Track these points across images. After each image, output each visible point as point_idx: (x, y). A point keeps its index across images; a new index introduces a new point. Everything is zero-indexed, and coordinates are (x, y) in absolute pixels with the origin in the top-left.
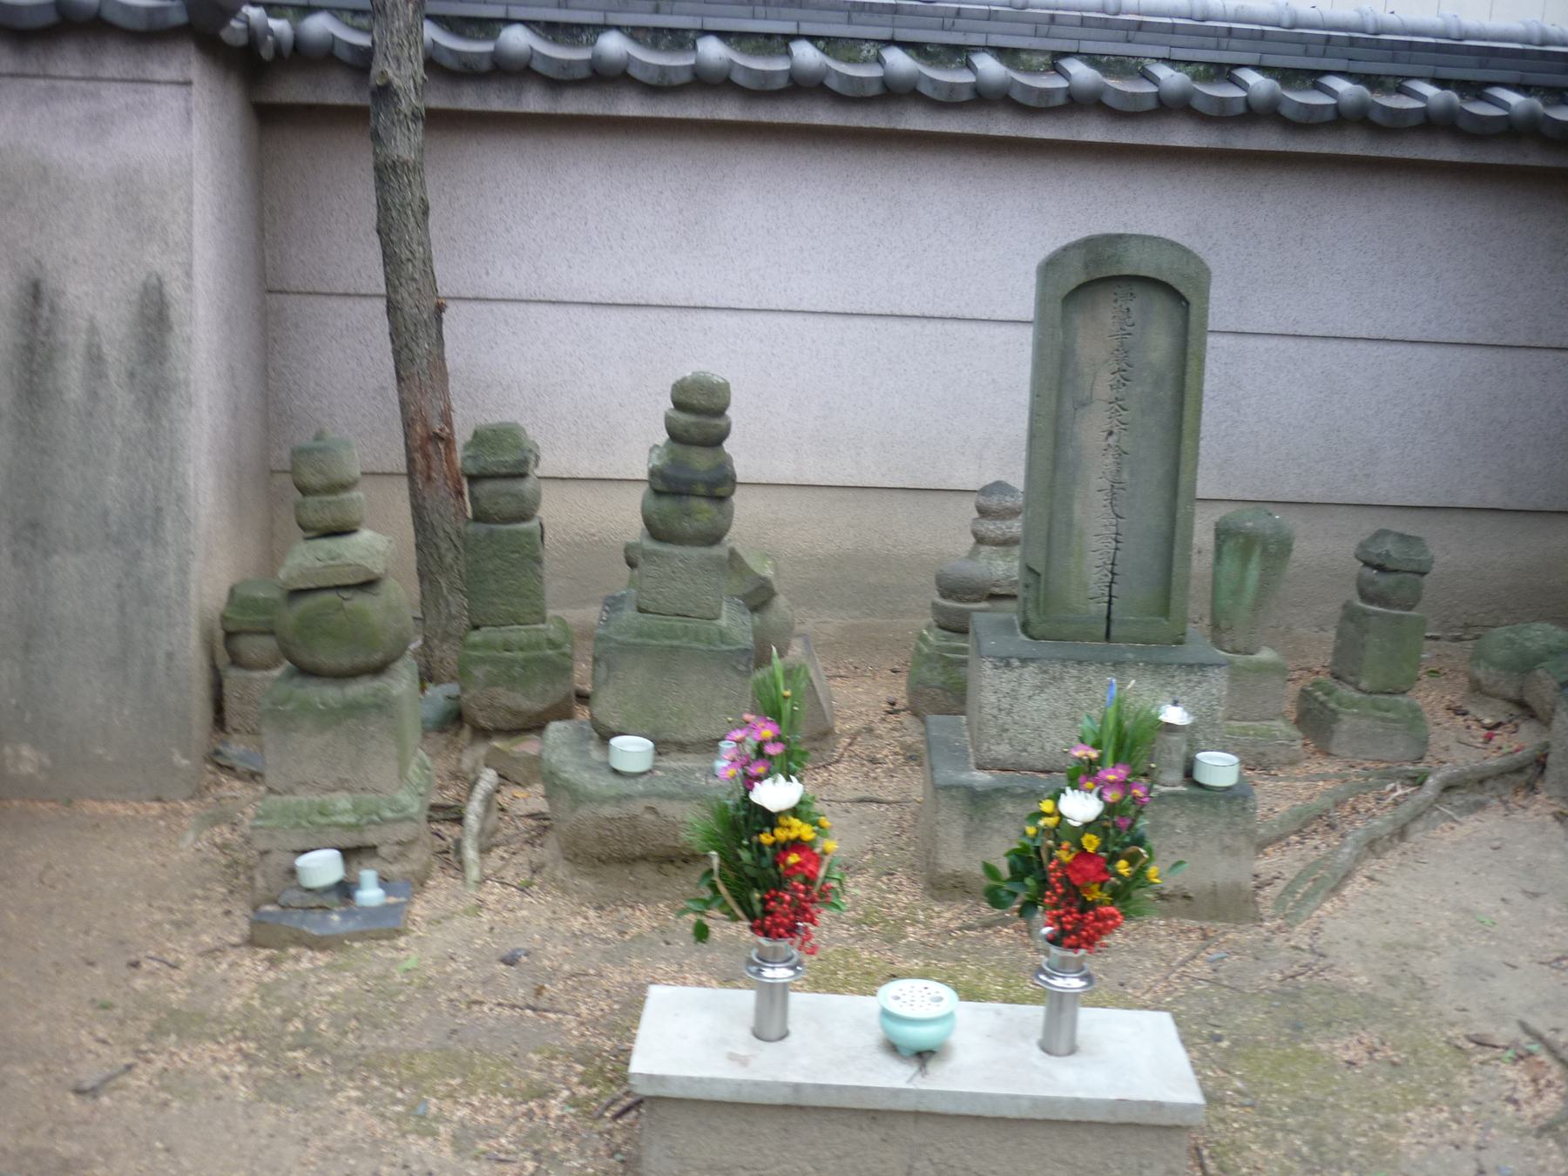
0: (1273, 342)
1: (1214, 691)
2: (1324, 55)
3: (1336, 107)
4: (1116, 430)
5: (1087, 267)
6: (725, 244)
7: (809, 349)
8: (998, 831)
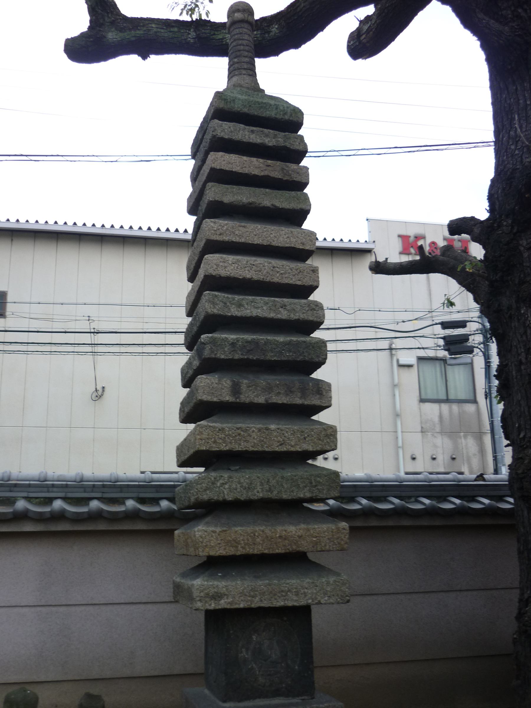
0: (83, 608)
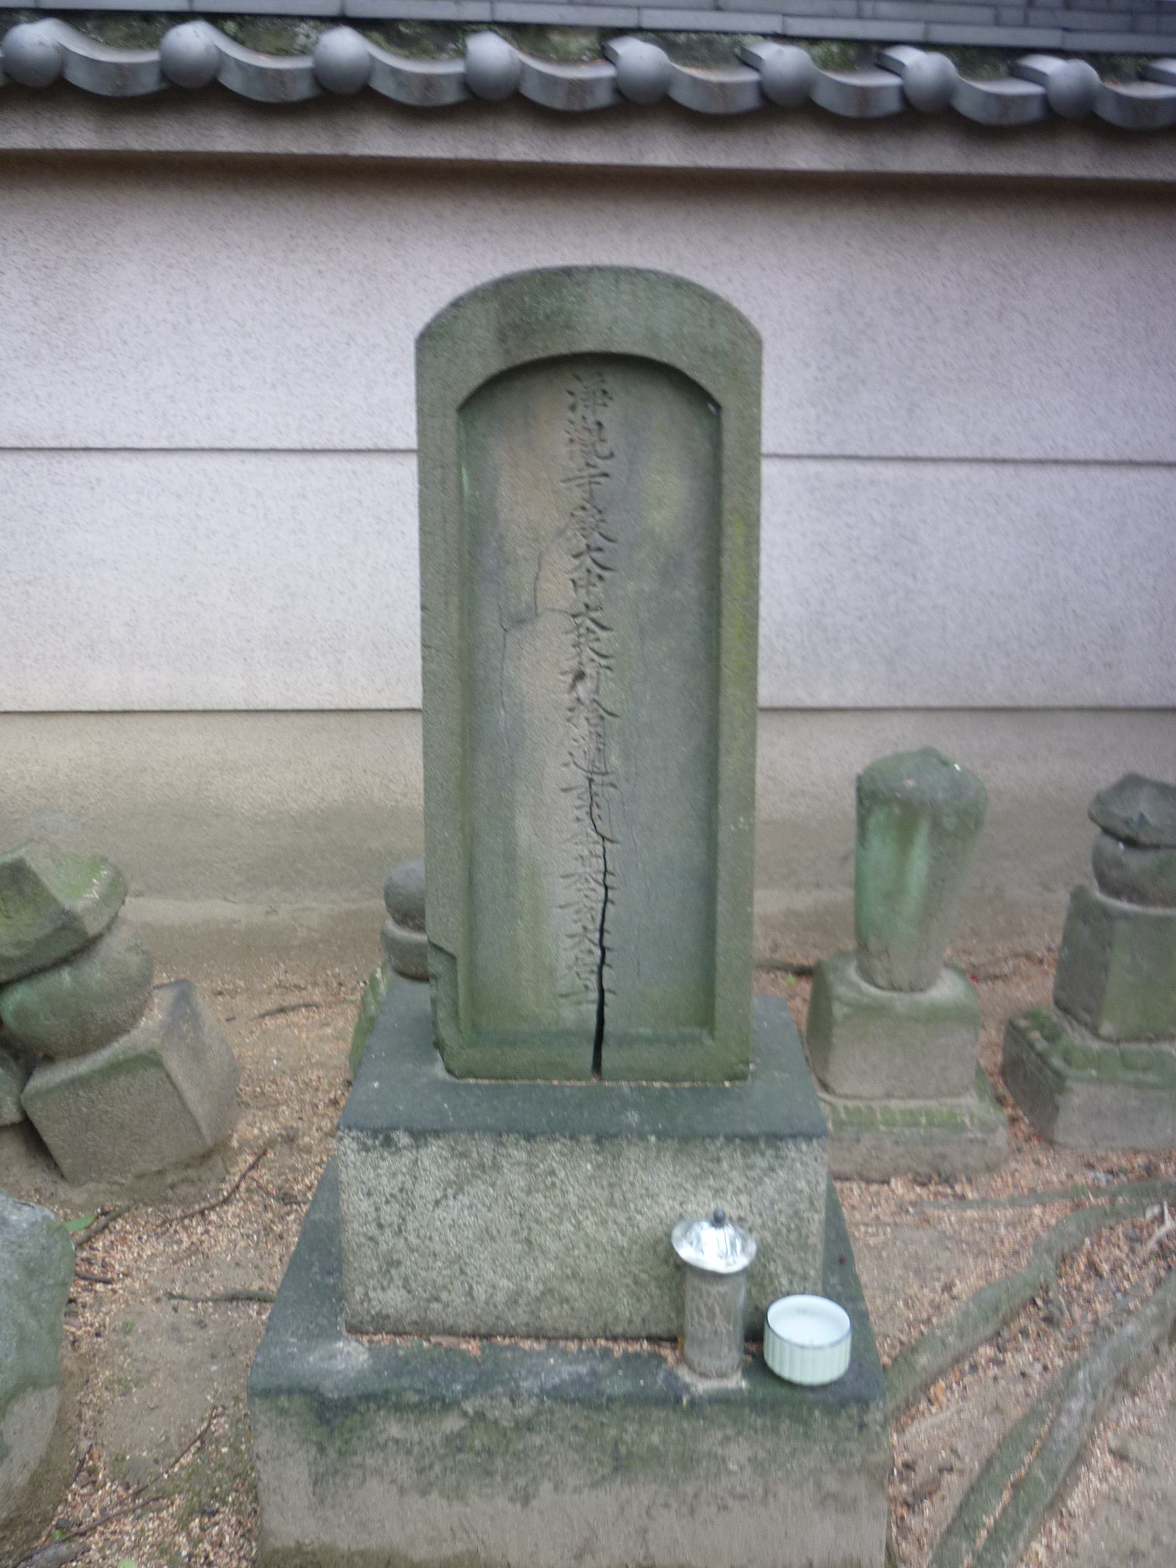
0: (962, 471)
1: (802, 1184)
2: (1025, 24)
3: (1045, 100)
4: (588, 670)
5: (503, 339)
6: (109, 350)
7: (254, 506)
8: (377, 1472)
